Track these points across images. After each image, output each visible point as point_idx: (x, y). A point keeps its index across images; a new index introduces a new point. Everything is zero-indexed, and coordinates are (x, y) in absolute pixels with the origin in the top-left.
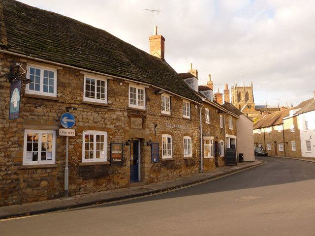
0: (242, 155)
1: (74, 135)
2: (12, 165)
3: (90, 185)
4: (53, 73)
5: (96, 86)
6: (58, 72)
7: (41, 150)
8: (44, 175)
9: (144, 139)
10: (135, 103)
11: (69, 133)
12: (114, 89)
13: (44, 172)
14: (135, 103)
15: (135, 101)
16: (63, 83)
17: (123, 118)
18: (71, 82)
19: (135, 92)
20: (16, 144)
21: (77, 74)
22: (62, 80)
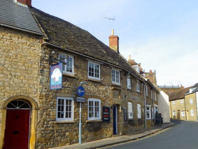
6: (74, 59)
15: (93, 74)
22: (77, 64)
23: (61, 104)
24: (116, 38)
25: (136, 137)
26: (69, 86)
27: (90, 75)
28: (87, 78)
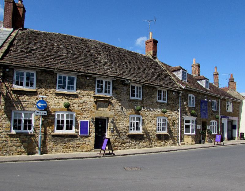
0: (243, 133)
1: (46, 115)
2: (3, 132)
3: (60, 147)
4: (34, 73)
5: (67, 81)
6: (37, 73)
7: (65, 124)
8: (25, 139)
9: (206, 122)
10: (134, 96)
11: (43, 113)
12: (82, 82)
13: (25, 137)
14: (134, 96)
15: (134, 95)
16: (40, 80)
17: (89, 102)
18: (46, 79)
19: (161, 92)
20: (5, 119)
21: (51, 73)
22: (39, 78)
23: (59, 119)
24: (197, 67)
25: (85, 152)
26: (27, 100)
27: (159, 99)
28: (129, 98)
